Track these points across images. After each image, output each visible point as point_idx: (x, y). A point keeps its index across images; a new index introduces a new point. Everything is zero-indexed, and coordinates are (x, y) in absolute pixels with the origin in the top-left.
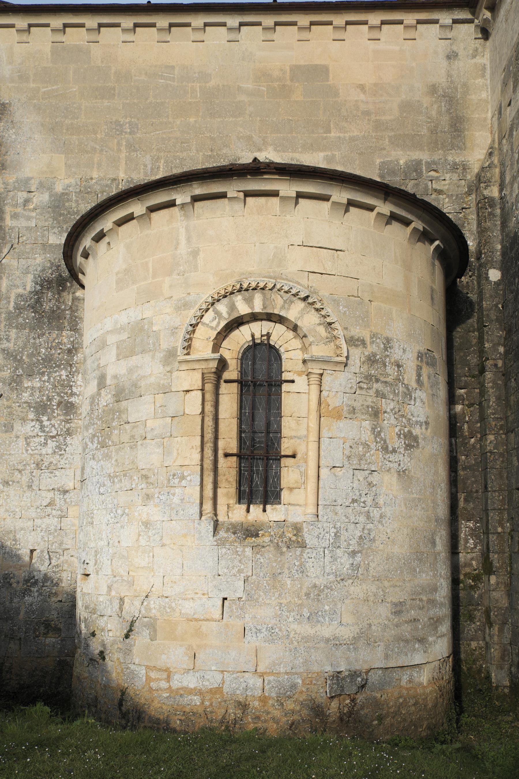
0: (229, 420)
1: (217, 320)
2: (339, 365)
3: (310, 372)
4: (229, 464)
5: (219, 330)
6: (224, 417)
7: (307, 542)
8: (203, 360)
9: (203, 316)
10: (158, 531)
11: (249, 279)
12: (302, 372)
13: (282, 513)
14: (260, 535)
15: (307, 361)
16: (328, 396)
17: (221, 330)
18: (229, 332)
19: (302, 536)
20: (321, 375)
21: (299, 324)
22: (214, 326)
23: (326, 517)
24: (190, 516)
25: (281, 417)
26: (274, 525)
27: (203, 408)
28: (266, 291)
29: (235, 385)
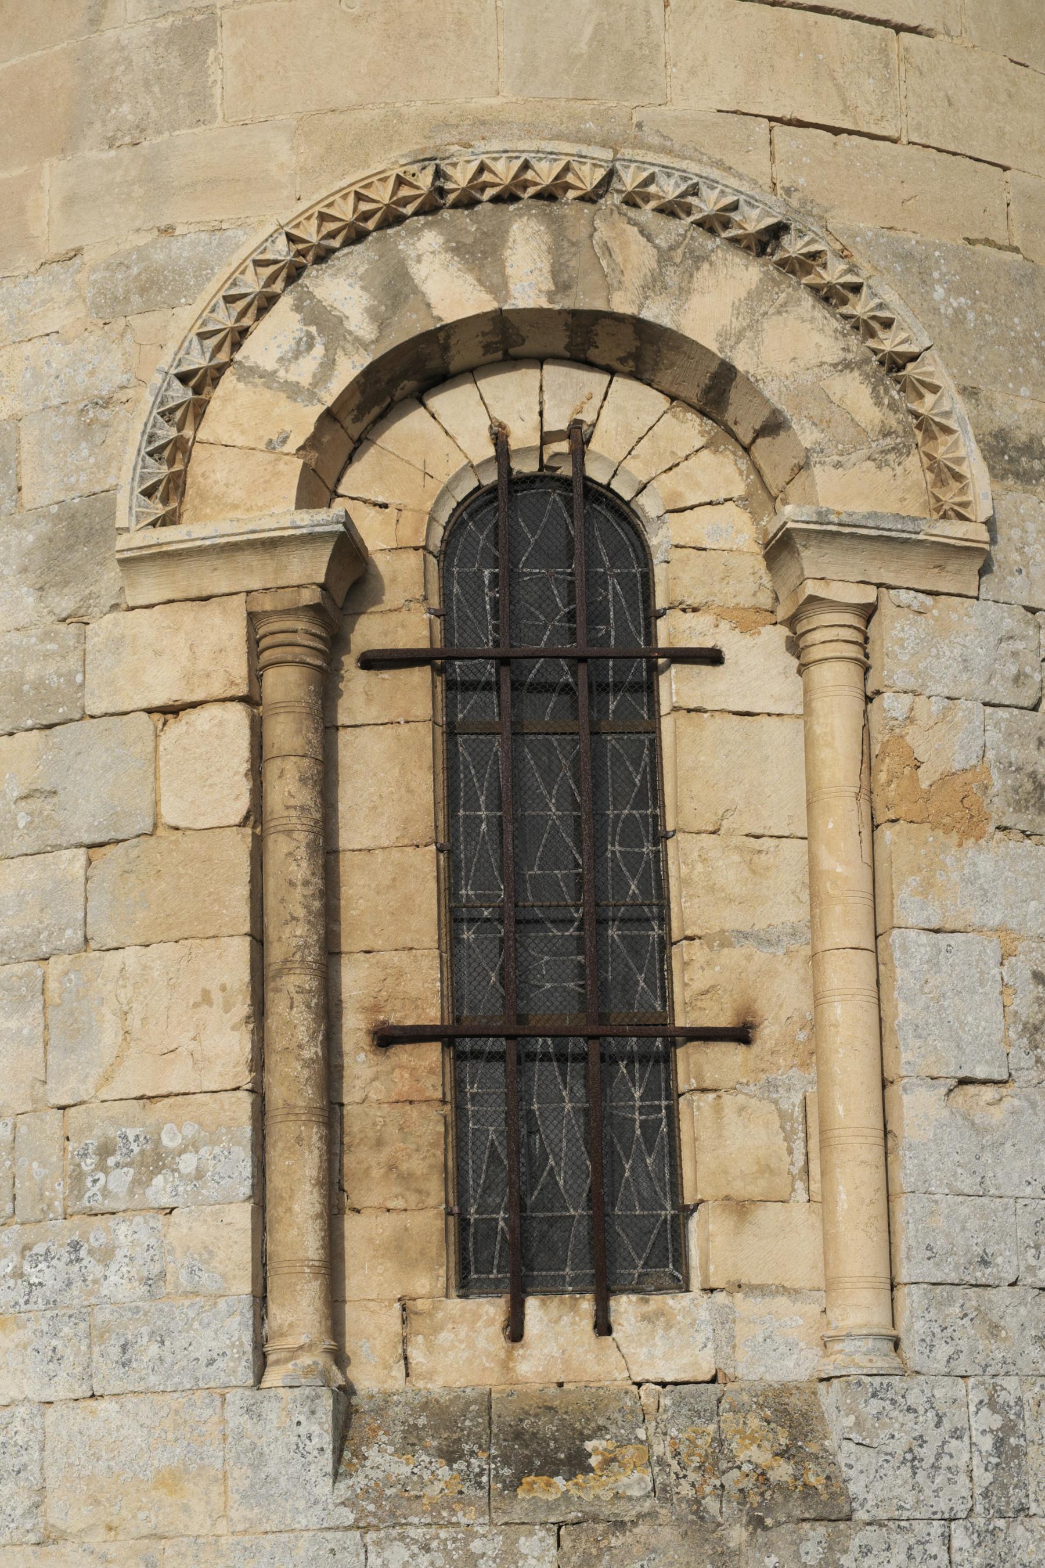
0: (396, 854)
1: (319, 350)
2: (952, 566)
3: (812, 599)
4: (402, 1084)
5: (329, 400)
6: (367, 843)
7: (853, 1488)
8: (251, 544)
9: (244, 332)
10: (17, 1463)
11: (480, 146)
12: (758, 610)
13: (700, 1338)
14: (594, 1461)
15: (799, 542)
16: (910, 719)
17: (342, 399)
18: (375, 422)
19: (824, 1458)
20: (868, 612)
21: (740, 365)
22: (305, 381)
23: (943, 1351)
24: (202, 1370)
25: (661, 837)
26: (666, 1401)
27: (258, 793)
28: (568, 204)
29: (420, 677)
